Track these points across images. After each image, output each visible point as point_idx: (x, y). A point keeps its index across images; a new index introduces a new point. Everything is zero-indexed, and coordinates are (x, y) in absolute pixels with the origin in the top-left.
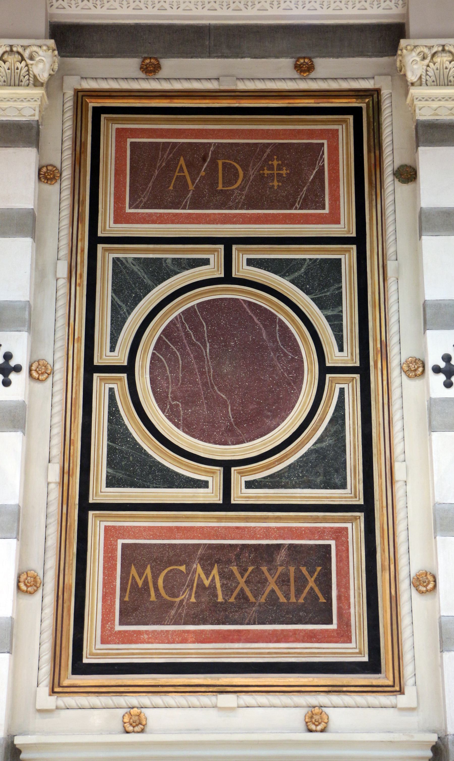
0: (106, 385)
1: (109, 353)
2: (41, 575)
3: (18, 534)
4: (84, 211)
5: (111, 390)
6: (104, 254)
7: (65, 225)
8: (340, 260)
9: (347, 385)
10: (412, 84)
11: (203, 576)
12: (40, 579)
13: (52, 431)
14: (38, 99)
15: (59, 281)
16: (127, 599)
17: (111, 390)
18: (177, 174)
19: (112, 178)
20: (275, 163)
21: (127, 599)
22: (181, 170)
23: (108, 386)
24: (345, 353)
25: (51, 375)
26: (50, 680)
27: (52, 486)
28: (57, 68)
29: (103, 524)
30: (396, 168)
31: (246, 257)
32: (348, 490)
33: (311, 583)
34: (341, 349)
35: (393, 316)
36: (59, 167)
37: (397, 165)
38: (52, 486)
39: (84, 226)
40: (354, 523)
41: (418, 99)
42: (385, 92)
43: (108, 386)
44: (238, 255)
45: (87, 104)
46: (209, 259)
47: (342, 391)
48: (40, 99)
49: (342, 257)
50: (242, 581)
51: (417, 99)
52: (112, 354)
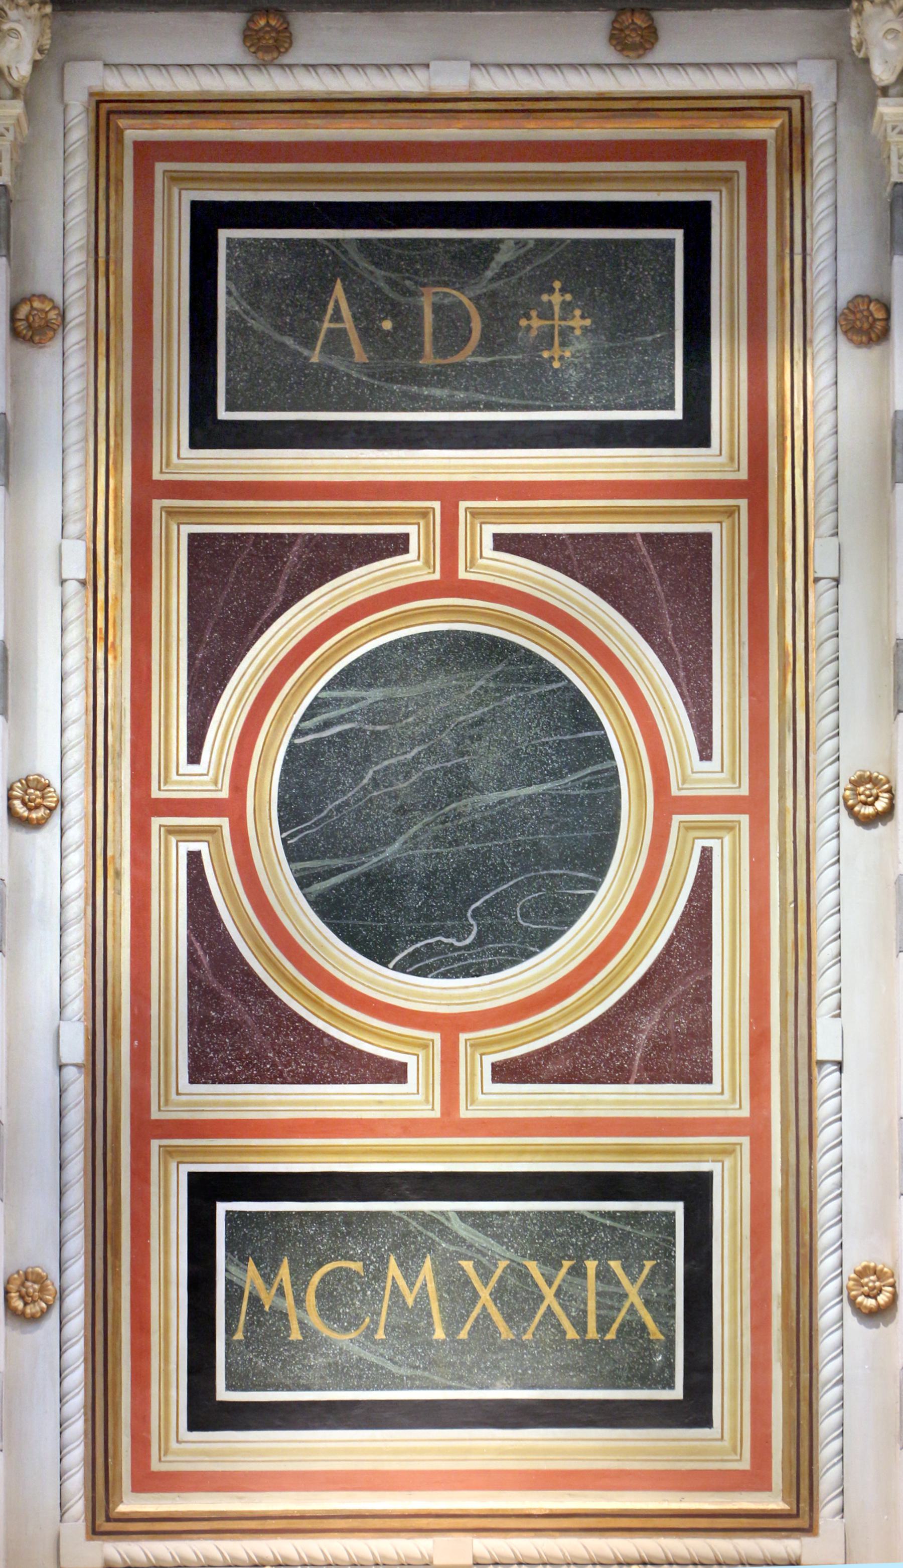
0: (182, 527)
1: (185, 768)
2: (56, 783)
3: (8, 249)
4: (120, 239)
5: (194, 858)
6: (170, 189)
7: (78, 216)
8: (706, 539)
9: (720, 1164)
10: (885, 91)
11: (402, 1283)
12: (53, 1284)
13: (66, 760)
14: (8, 130)
15: (67, 584)
16: (239, 1336)
17: (194, 858)
18: (326, 325)
19: (181, 720)
20: (556, 299)
21: (239, 1336)
22: (337, 317)
23: (185, 848)
24: (714, 764)
25: (58, 811)
26: (85, 1003)
27: (72, 587)
28: (49, 42)
29: (187, 529)
30: (842, 304)
31: (489, 531)
32: (715, 1087)
33: (634, 1297)
34: (705, 753)
35: (821, 398)
36: (58, 300)
37: (845, 295)
38: (71, 1073)
39: (120, 363)
40: (724, 525)
41: (897, 130)
42: (820, 107)
43: (185, 848)
44: (472, 525)
45: (120, 132)
46: (405, 1065)
47: (706, 856)
48: (12, 129)
49: (713, 528)
50: (485, 1294)
51: (893, 128)
52: (194, 769)
